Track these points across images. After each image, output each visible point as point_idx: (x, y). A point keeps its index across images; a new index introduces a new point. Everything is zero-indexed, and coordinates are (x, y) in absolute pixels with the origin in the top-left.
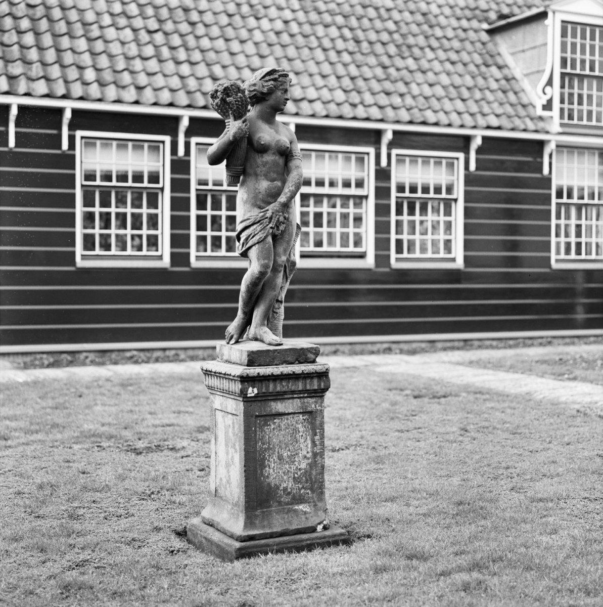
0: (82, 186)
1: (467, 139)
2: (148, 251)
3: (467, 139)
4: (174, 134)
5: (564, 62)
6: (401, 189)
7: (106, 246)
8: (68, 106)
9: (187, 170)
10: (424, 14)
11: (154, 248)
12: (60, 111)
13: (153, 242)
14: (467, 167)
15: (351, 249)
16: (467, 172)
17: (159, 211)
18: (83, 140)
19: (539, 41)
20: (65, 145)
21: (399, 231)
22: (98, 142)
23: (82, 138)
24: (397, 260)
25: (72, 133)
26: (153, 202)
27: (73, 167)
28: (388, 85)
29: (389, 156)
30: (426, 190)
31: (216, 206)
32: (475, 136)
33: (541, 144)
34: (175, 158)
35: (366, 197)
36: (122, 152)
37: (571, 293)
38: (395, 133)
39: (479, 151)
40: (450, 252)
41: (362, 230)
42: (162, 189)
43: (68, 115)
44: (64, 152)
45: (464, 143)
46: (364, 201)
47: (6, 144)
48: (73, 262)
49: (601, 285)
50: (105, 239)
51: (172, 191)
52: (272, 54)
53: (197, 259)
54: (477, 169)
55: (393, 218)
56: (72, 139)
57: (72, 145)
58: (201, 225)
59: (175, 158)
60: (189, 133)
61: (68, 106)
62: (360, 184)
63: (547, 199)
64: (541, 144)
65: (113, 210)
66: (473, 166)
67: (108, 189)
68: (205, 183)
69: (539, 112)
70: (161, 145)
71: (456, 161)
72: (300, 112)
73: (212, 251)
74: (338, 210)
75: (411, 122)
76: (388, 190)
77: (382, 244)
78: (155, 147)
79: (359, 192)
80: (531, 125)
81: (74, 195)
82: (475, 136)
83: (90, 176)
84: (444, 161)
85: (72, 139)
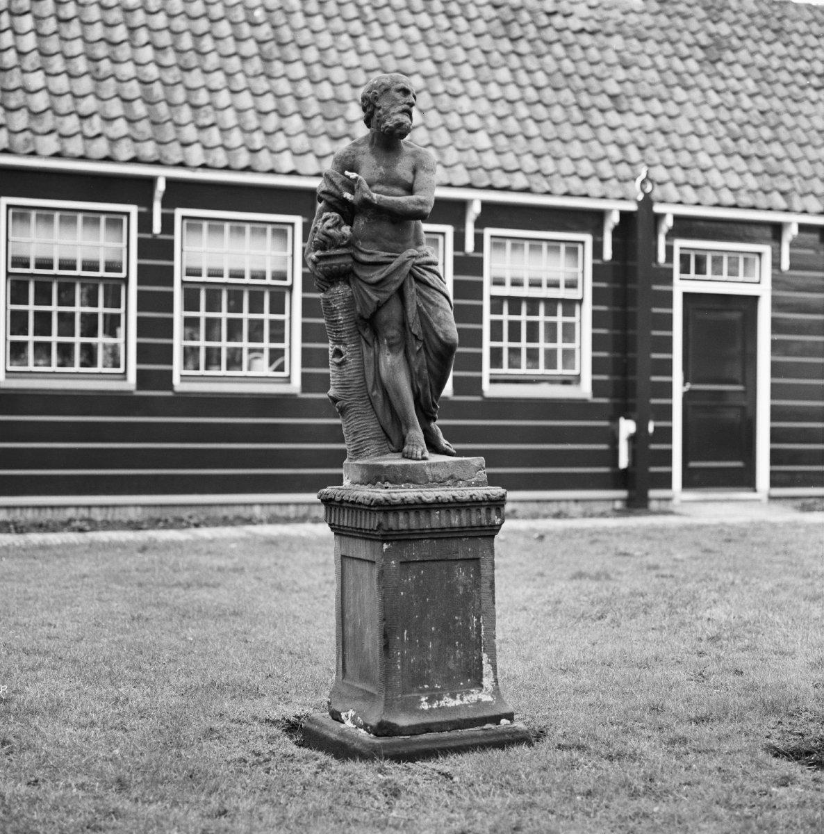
0: (183, 282)
1: (777, 230)
2: (36, 365)
3: (600, 215)
4: (459, 224)
8: (162, 175)
10: (761, 69)
11: (217, 367)
12: (151, 181)
14: (776, 264)
15: (560, 370)
16: (776, 272)
17: (122, 310)
18: (185, 222)
22: (205, 224)
23: (184, 218)
24: (493, 381)
25: (479, 231)
26: (114, 298)
27: (480, 273)
31: (256, 307)
32: (789, 224)
34: (598, 262)
35: (580, 302)
36: (517, 255)
38: (677, 218)
40: (116, 365)
42: (291, 288)
43: (161, 186)
44: (155, 236)
45: (592, 220)
46: (577, 308)
49: (821, 425)
51: (140, 282)
52: (513, 114)
53: (182, 379)
54: (792, 267)
56: (479, 239)
57: (669, 258)
59: (460, 254)
60: (480, 223)
61: (162, 175)
62: (571, 285)
65: (54, 308)
66: (785, 264)
67: (25, 278)
68: (49, 265)
70: (125, 219)
71: (289, 229)
72: (685, 200)
73: (228, 369)
74: (524, 318)
78: (115, 221)
81: (171, 295)
82: (789, 224)
83: (498, 282)
84: (563, 246)
85: (479, 239)
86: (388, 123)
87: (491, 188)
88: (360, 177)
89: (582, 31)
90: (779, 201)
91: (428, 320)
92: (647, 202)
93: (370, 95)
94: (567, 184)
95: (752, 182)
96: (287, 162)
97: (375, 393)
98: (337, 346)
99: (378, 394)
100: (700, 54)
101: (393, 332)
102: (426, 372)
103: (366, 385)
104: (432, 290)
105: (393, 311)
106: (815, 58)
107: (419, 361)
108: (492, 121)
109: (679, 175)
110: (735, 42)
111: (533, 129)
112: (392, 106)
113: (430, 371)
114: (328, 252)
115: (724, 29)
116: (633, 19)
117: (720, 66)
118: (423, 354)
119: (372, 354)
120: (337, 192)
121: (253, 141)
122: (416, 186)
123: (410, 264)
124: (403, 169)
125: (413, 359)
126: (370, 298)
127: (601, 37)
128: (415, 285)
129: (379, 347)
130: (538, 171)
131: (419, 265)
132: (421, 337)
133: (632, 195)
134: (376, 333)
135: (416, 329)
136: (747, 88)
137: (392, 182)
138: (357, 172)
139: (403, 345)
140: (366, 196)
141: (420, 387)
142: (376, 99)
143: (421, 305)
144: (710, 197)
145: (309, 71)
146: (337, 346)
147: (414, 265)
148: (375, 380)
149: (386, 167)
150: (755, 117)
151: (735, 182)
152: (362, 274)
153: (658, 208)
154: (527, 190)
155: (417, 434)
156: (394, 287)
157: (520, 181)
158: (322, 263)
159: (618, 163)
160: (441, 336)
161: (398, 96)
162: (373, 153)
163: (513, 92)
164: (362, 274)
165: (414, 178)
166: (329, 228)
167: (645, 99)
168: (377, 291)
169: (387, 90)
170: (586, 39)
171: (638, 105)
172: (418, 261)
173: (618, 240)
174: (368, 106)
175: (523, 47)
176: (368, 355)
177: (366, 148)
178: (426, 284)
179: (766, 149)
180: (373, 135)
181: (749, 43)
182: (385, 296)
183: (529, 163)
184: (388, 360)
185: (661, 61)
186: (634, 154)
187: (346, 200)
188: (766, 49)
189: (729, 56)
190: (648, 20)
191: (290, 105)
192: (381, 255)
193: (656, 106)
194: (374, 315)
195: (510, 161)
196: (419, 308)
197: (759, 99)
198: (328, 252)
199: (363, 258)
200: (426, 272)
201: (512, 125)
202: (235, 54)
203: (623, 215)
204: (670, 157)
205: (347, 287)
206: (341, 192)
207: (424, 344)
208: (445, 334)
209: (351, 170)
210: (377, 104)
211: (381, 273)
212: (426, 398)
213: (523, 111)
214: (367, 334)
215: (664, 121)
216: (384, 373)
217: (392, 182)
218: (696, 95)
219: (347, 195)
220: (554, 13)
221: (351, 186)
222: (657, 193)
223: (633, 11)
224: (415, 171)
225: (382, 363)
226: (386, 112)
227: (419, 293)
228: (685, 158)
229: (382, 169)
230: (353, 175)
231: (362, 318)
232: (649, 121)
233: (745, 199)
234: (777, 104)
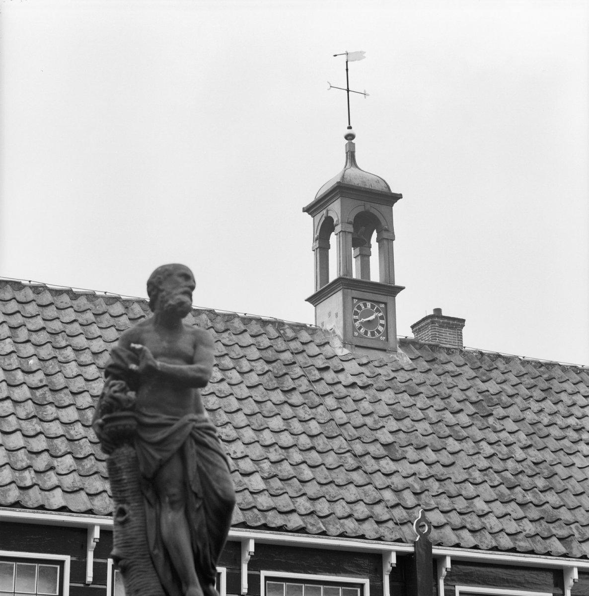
3: (378, 557)
86: (171, 302)
87: (265, 527)
88: (145, 348)
89: (353, 385)
90: (559, 547)
91: (207, 479)
92: (425, 544)
93: (154, 280)
94: (342, 525)
95: (530, 528)
96: (57, 499)
97: (156, 552)
98: (121, 506)
99: (159, 553)
100: (472, 409)
101: (174, 490)
102: (205, 530)
103: (148, 543)
104: (213, 452)
105: (175, 469)
106: (584, 416)
107: (199, 518)
108: (266, 465)
109: (456, 519)
110: (504, 398)
111: (307, 474)
112: (174, 288)
113: (209, 530)
114: (115, 414)
115: (492, 387)
116: (401, 376)
117: (491, 420)
118: (202, 511)
119: (154, 514)
120: (123, 365)
121: (24, 479)
122: (196, 358)
123: (190, 426)
124: (184, 344)
125: (193, 515)
126: (153, 457)
127: (372, 391)
128: (195, 446)
129: (161, 506)
130: (312, 513)
131: (199, 428)
132: (201, 495)
133: (409, 538)
134: (158, 495)
135: (196, 487)
136: (519, 441)
137: (174, 354)
138: (142, 343)
139: (185, 504)
140: (150, 363)
141: (200, 546)
142: (160, 283)
143: (201, 464)
144: (489, 541)
145: (81, 416)
146: (121, 506)
147: (194, 428)
148: (156, 540)
149: (169, 342)
150: (527, 467)
151: (512, 527)
152: (146, 435)
153: (436, 551)
154: (302, 530)
155: (197, 590)
156: (175, 447)
157: (295, 521)
158: (109, 425)
159: (393, 507)
160: (220, 492)
161: (180, 280)
162: (156, 331)
163: (286, 439)
164: (146, 435)
165: (195, 352)
166: (115, 392)
167: (420, 448)
168: (158, 450)
169: (170, 275)
170: (358, 393)
171: (411, 454)
172: (198, 425)
173: (397, 584)
174: (153, 290)
175: (296, 398)
176: (151, 514)
177: (150, 327)
178: (206, 446)
179: (544, 497)
180: (157, 316)
181: (518, 400)
182: (167, 455)
183: (303, 505)
184: (170, 517)
185: (432, 414)
186: (409, 499)
187: (132, 371)
188: (535, 407)
189: (499, 411)
190: (418, 377)
191: (62, 445)
192: (163, 418)
193: (429, 455)
194: (156, 474)
195: (283, 502)
196: (199, 469)
197: (531, 451)
198: (115, 414)
199: (147, 420)
200: (205, 435)
201: (286, 469)
202: (8, 398)
203: (400, 556)
204: (445, 502)
205: (131, 449)
206: (127, 365)
207: (204, 503)
208: (223, 491)
209: (137, 342)
210: (161, 287)
211: (164, 433)
212: (205, 558)
213: (297, 457)
214: (149, 494)
215: (438, 470)
216: (165, 530)
217: (174, 354)
218: (468, 446)
219: (133, 367)
220: (327, 369)
221: (137, 356)
222: (435, 535)
223: (404, 432)
224: (195, 347)
225: (163, 521)
226: (169, 293)
227: (199, 454)
228: (460, 504)
229: (165, 344)
230: (138, 346)
231: (145, 478)
232: (422, 468)
233: (524, 544)
234: (548, 456)
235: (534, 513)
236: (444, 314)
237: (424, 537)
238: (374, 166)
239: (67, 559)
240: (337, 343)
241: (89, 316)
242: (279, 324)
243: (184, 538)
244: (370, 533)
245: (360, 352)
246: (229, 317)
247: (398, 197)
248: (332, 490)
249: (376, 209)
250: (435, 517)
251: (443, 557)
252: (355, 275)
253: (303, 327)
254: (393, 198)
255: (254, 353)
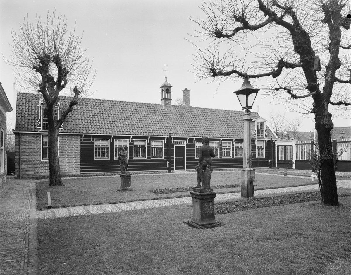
4: (164, 140)
5: (258, 128)
6: (235, 147)
7: (226, 155)
9: (234, 146)
13: (144, 156)
19: (254, 125)
20: (194, 143)
21: (196, 153)
28: (233, 132)
29: (221, 142)
30: (239, 147)
31: (99, 149)
33: (255, 140)
37: (257, 162)
39: (189, 140)
41: (230, 153)
43: (131, 137)
47: (172, 142)
48: (114, 159)
50: (226, 154)
51: (164, 148)
55: (235, 151)
57: (195, 143)
58: (152, 152)
61: (131, 136)
63: (255, 148)
64: (255, 140)
69: (254, 135)
75: (237, 138)
76: (234, 147)
77: (233, 155)
79: (230, 148)
80: (253, 138)
85: (195, 142)
87: (151, 135)
92: (170, 136)
95: (184, 133)
101: (124, 163)
105: (124, 162)
107: (126, 165)
139: (124, 164)
153: (171, 137)
163: (155, 122)
171: (171, 123)
183: (156, 132)
189: (183, 116)
190: (173, 111)
191: (127, 125)
213: (156, 125)
228: (176, 130)
233: (183, 135)
235: (185, 131)
236: (187, 89)
237: (170, 135)
238: (170, 82)
239: (128, 140)
240: (163, 107)
241: (131, 106)
242: (156, 104)
243: (124, 167)
244: (164, 135)
245: (166, 108)
246: (149, 104)
247: (172, 86)
248: (160, 129)
249: (169, 88)
250: (172, 132)
251: (172, 137)
252: (166, 98)
253: (159, 104)
254: (171, 87)
255: (152, 110)
